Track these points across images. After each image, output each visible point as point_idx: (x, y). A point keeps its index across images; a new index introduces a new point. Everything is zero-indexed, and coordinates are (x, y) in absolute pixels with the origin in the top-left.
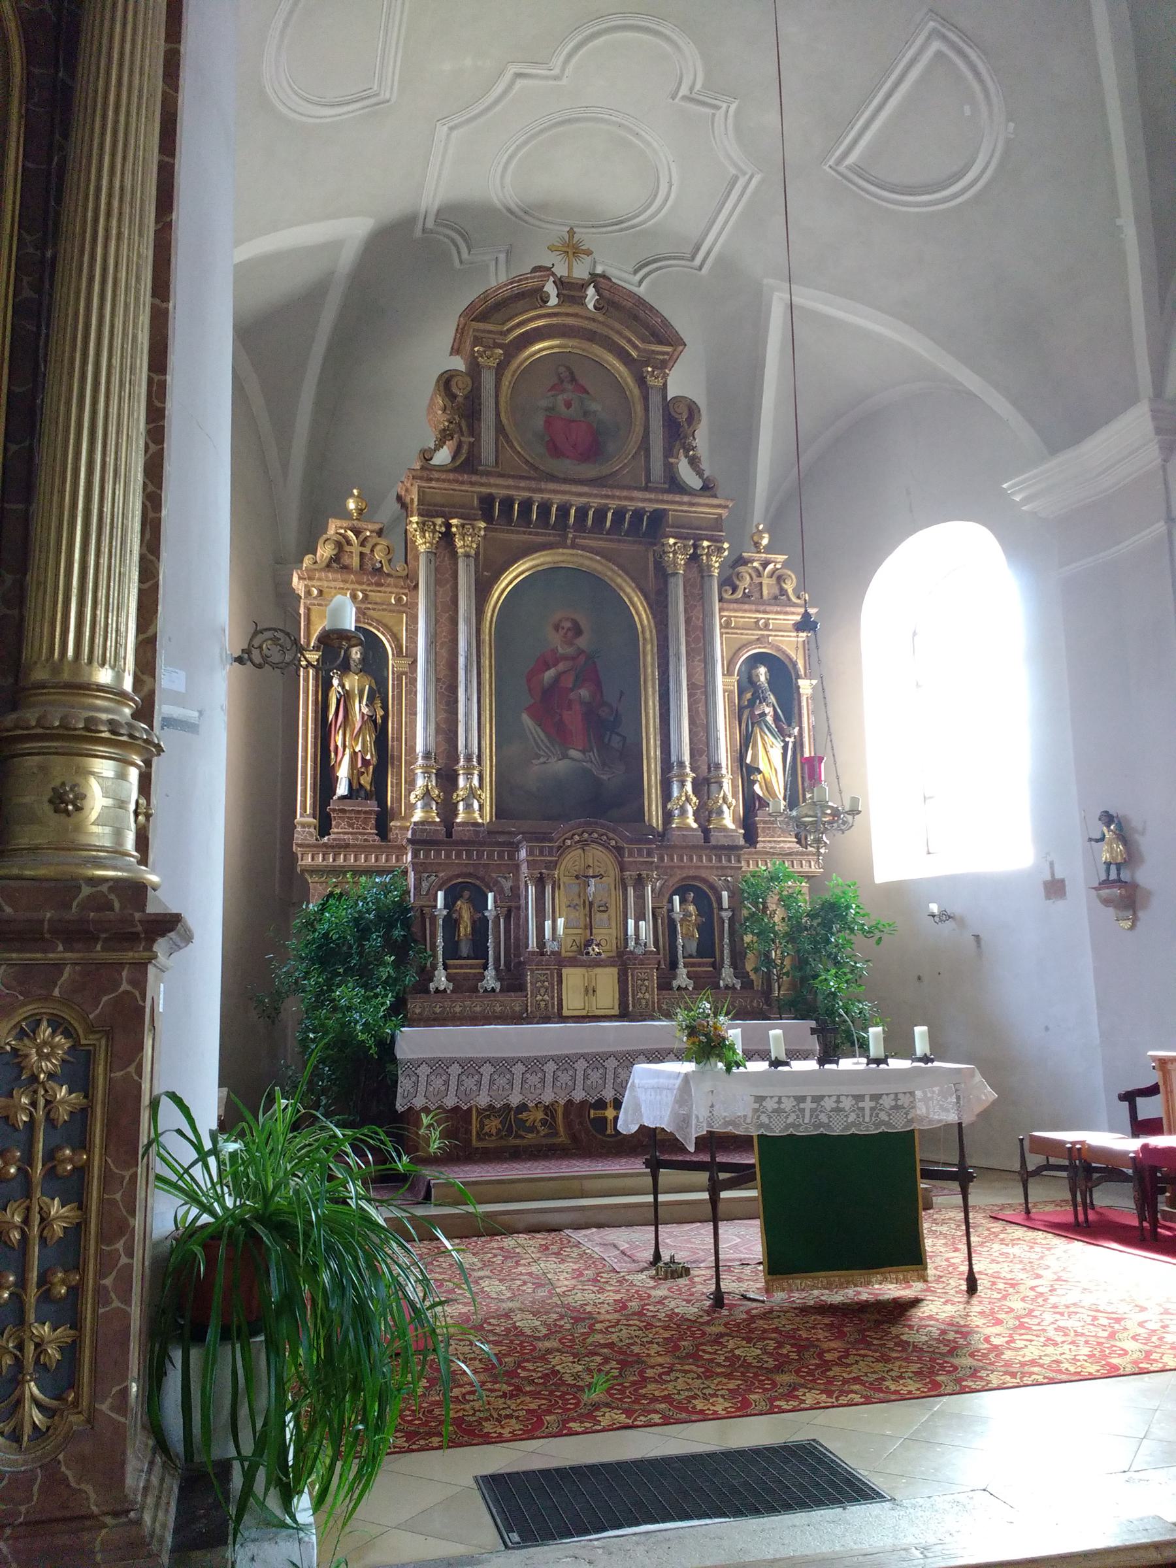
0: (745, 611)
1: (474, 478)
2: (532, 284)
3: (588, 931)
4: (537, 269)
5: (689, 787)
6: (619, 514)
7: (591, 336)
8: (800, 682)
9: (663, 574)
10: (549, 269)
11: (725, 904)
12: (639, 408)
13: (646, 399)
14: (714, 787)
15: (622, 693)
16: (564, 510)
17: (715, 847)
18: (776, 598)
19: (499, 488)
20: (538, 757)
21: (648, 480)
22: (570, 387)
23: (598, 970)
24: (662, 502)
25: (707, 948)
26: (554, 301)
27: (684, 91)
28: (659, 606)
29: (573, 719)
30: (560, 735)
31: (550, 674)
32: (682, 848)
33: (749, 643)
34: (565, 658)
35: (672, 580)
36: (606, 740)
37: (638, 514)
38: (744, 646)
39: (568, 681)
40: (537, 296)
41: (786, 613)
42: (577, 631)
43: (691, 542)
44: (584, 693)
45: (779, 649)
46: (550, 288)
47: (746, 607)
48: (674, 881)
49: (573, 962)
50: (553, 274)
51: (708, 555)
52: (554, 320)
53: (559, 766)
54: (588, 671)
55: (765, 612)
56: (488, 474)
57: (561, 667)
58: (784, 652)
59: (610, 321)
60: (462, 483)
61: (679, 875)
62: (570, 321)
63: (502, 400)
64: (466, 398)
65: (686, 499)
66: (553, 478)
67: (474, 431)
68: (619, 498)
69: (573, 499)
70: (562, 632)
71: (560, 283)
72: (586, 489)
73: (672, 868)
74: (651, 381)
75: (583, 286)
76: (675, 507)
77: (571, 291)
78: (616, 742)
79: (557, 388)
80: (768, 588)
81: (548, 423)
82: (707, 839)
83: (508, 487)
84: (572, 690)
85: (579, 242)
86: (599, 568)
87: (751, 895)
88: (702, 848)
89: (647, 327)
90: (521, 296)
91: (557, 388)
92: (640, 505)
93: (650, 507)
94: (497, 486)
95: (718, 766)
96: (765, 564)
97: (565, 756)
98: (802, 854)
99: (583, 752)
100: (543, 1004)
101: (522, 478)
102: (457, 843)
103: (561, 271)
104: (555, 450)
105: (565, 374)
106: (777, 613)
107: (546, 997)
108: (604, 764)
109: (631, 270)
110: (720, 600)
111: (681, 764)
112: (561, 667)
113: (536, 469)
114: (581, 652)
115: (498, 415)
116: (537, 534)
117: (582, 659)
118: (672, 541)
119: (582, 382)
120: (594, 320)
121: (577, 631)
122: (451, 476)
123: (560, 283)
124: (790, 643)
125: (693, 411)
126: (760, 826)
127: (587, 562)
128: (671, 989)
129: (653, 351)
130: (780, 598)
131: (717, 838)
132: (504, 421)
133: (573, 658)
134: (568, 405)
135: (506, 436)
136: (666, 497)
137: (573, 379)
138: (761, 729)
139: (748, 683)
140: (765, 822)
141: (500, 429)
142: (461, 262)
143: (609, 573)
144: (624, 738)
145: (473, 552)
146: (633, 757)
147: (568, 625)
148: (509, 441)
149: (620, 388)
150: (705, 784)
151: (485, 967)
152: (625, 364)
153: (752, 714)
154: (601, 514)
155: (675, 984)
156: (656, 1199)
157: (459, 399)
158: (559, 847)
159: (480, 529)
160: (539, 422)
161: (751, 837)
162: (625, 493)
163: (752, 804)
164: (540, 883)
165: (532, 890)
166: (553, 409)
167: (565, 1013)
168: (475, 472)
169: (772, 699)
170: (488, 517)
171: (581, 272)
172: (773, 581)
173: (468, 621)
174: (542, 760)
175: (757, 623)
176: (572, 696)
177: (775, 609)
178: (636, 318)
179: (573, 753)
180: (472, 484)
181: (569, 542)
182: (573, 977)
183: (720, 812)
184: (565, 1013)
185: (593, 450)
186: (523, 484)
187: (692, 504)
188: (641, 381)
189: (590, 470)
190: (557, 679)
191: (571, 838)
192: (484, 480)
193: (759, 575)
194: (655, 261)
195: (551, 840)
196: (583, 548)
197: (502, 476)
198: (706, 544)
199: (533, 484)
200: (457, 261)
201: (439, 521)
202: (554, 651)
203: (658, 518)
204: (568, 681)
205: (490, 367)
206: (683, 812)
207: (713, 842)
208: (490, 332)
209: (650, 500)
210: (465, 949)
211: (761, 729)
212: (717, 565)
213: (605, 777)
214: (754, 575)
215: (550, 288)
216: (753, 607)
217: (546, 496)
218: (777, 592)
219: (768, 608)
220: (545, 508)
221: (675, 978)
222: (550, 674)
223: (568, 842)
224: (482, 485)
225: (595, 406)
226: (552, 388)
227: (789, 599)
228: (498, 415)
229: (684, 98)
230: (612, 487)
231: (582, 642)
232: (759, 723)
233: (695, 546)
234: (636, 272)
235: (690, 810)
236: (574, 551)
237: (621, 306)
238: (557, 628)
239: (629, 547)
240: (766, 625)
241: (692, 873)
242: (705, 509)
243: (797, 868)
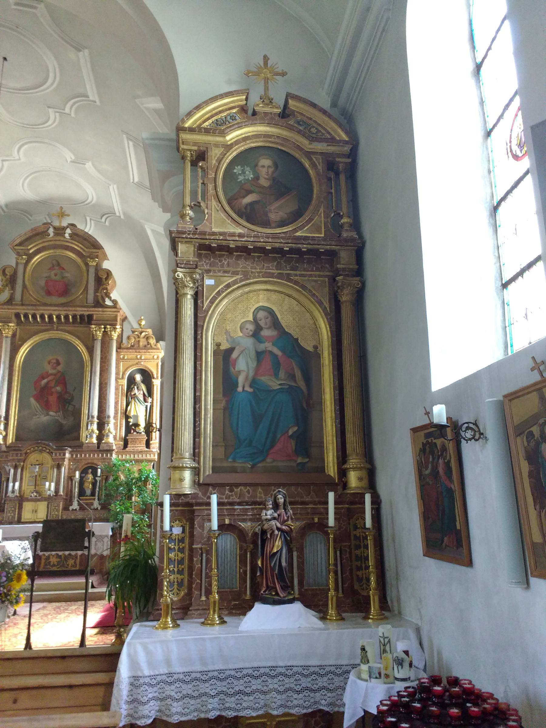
0: (130, 352)
1: (10, 307)
2: (42, 229)
3: (34, 487)
4: (44, 224)
5: (95, 427)
6: (74, 317)
7: (67, 248)
8: (153, 380)
9: (94, 339)
10: (50, 224)
11: (99, 474)
12: (85, 274)
13: (88, 271)
14: (106, 425)
15: (75, 388)
16: (50, 317)
17: (101, 451)
18: (145, 346)
19: (22, 310)
20: (36, 415)
21: (87, 303)
22: (57, 268)
23: (38, 503)
24: (91, 311)
25: (93, 494)
26: (52, 234)
27: (69, 160)
28: (91, 351)
29: (53, 399)
30: (47, 406)
31: (44, 382)
32: (86, 451)
33: (133, 365)
34: (51, 375)
35: (95, 342)
36: (66, 407)
37: (82, 316)
38: (130, 366)
39: (52, 384)
40: (44, 233)
41: (149, 352)
42: (58, 363)
43: (103, 326)
44: (58, 388)
45: (146, 367)
46: (51, 231)
47: (131, 350)
48: (82, 465)
49: (28, 500)
50: (52, 225)
51: (110, 331)
52: (51, 243)
53: (43, 418)
54: (62, 380)
55: (139, 352)
56: (17, 305)
57: (50, 378)
58: (148, 368)
59: (73, 242)
60: (5, 309)
61: (84, 462)
62: (58, 243)
63: (27, 276)
64: (11, 276)
65: (100, 309)
66: (45, 305)
67: (13, 288)
68: (71, 311)
69: (52, 312)
70: (51, 364)
71: (55, 228)
72: (57, 308)
73: (81, 460)
74: (90, 264)
75: (64, 229)
76: (97, 313)
77: (60, 231)
78: (70, 408)
79: (51, 269)
80: (143, 342)
81: (47, 283)
82: (98, 447)
83: (24, 309)
84: (53, 387)
85: (65, 211)
86: (69, 338)
87: (111, 470)
88: (95, 451)
89: (90, 242)
90: (37, 234)
91: (51, 269)
92: (82, 313)
93: (86, 313)
94: (20, 309)
95: (109, 417)
96: (141, 333)
97: (48, 415)
98: (147, 451)
99: (56, 412)
100: (11, 517)
101: (32, 305)
102: (101, 451)
103: (56, 224)
104: (49, 293)
105: (56, 264)
106: (145, 352)
107: (56, 513)
108: (65, 417)
109: (100, 217)
110: (119, 347)
111: (93, 417)
112: (50, 378)
113: (39, 301)
114: (59, 372)
115: (24, 281)
116: (42, 326)
117: (59, 375)
118: (93, 326)
119: (62, 265)
120: (67, 242)
121: (58, 363)
122: (5, 307)
123: (55, 228)
124: (154, 368)
125: (109, 274)
126: (129, 440)
127: (64, 336)
128: (69, 510)
129: (92, 252)
130: (148, 347)
131: (103, 446)
132: (27, 283)
133: (55, 375)
134: (56, 275)
135: (27, 289)
136: (91, 309)
137: (59, 264)
138: (135, 400)
139: (131, 381)
140: (132, 439)
141: (24, 286)
142: (30, 220)
143: (73, 340)
144: (75, 406)
145: (10, 335)
146: (77, 414)
147: (54, 361)
148: (28, 291)
149: (79, 266)
150: (101, 426)
151: (94, 499)
152: (80, 258)
153: (130, 394)
154: (66, 317)
155: (71, 508)
156: (32, 595)
157: (8, 277)
158: (26, 453)
159: (11, 326)
160: (42, 283)
161: (126, 445)
162: (74, 309)
163: (131, 428)
164: (16, 468)
165: (12, 471)
166: (49, 277)
167: (23, 520)
168: (12, 304)
169: (143, 387)
170: (19, 323)
171: (64, 224)
172: (145, 340)
173: (4, 363)
174: (38, 416)
175: (137, 357)
176: (53, 390)
177: (144, 351)
178: (85, 239)
179: (51, 413)
180: (8, 309)
181: (55, 328)
182: (28, 507)
183: (108, 436)
184: (23, 520)
185: (65, 291)
186: (29, 308)
187: (103, 311)
188: (87, 265)
189: (63, 300)
190: (48, 383)
191: (30, 449)
192: (13, 307)
193: (139, 337)
194: (107, 214)
195: (21, 450)
196: (61, 330)
197: (22, 305)
198: (108, 327)
199: (34, 308)
200: (29, 221)
201: (103, 326)
202: (47, 372)
203: (90, 317)
204: (52, 384)
205: (21, 263)
206: (91, 436)
207: (101, 448)
208: (22, 249)
209: (85, 311)
210: (88, 492)
211: (135, 400)
212: (100, 334)
213: (65, 422)
214: (136, 337)
215: (51, 231)
216: (134, 351)
217: (41, 312)
218: (146, 343)
219: (141, 351)
220: (42, 317)
221: (71, 505)
222: (44, 382)
223: (28, 451)
224: (13, 309)
225: (67, 275)
226: (50, 269)
227: (151, 346)
228: (24, 281)
229: (71, 162)
230: (71, 306)
231: (60, 368)
232: (134, 398)
233: (105, 328)
234: (101, 218)
235: (95, 436)
236: (57, 332)
237: (79, 236)
238: (49, 363)
239: (81, 329)
240: (141, 357)
241: (90, 461)
242: (109, 313)
243: (144, 457)
